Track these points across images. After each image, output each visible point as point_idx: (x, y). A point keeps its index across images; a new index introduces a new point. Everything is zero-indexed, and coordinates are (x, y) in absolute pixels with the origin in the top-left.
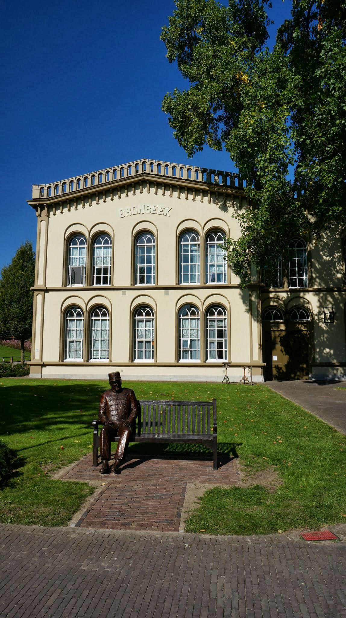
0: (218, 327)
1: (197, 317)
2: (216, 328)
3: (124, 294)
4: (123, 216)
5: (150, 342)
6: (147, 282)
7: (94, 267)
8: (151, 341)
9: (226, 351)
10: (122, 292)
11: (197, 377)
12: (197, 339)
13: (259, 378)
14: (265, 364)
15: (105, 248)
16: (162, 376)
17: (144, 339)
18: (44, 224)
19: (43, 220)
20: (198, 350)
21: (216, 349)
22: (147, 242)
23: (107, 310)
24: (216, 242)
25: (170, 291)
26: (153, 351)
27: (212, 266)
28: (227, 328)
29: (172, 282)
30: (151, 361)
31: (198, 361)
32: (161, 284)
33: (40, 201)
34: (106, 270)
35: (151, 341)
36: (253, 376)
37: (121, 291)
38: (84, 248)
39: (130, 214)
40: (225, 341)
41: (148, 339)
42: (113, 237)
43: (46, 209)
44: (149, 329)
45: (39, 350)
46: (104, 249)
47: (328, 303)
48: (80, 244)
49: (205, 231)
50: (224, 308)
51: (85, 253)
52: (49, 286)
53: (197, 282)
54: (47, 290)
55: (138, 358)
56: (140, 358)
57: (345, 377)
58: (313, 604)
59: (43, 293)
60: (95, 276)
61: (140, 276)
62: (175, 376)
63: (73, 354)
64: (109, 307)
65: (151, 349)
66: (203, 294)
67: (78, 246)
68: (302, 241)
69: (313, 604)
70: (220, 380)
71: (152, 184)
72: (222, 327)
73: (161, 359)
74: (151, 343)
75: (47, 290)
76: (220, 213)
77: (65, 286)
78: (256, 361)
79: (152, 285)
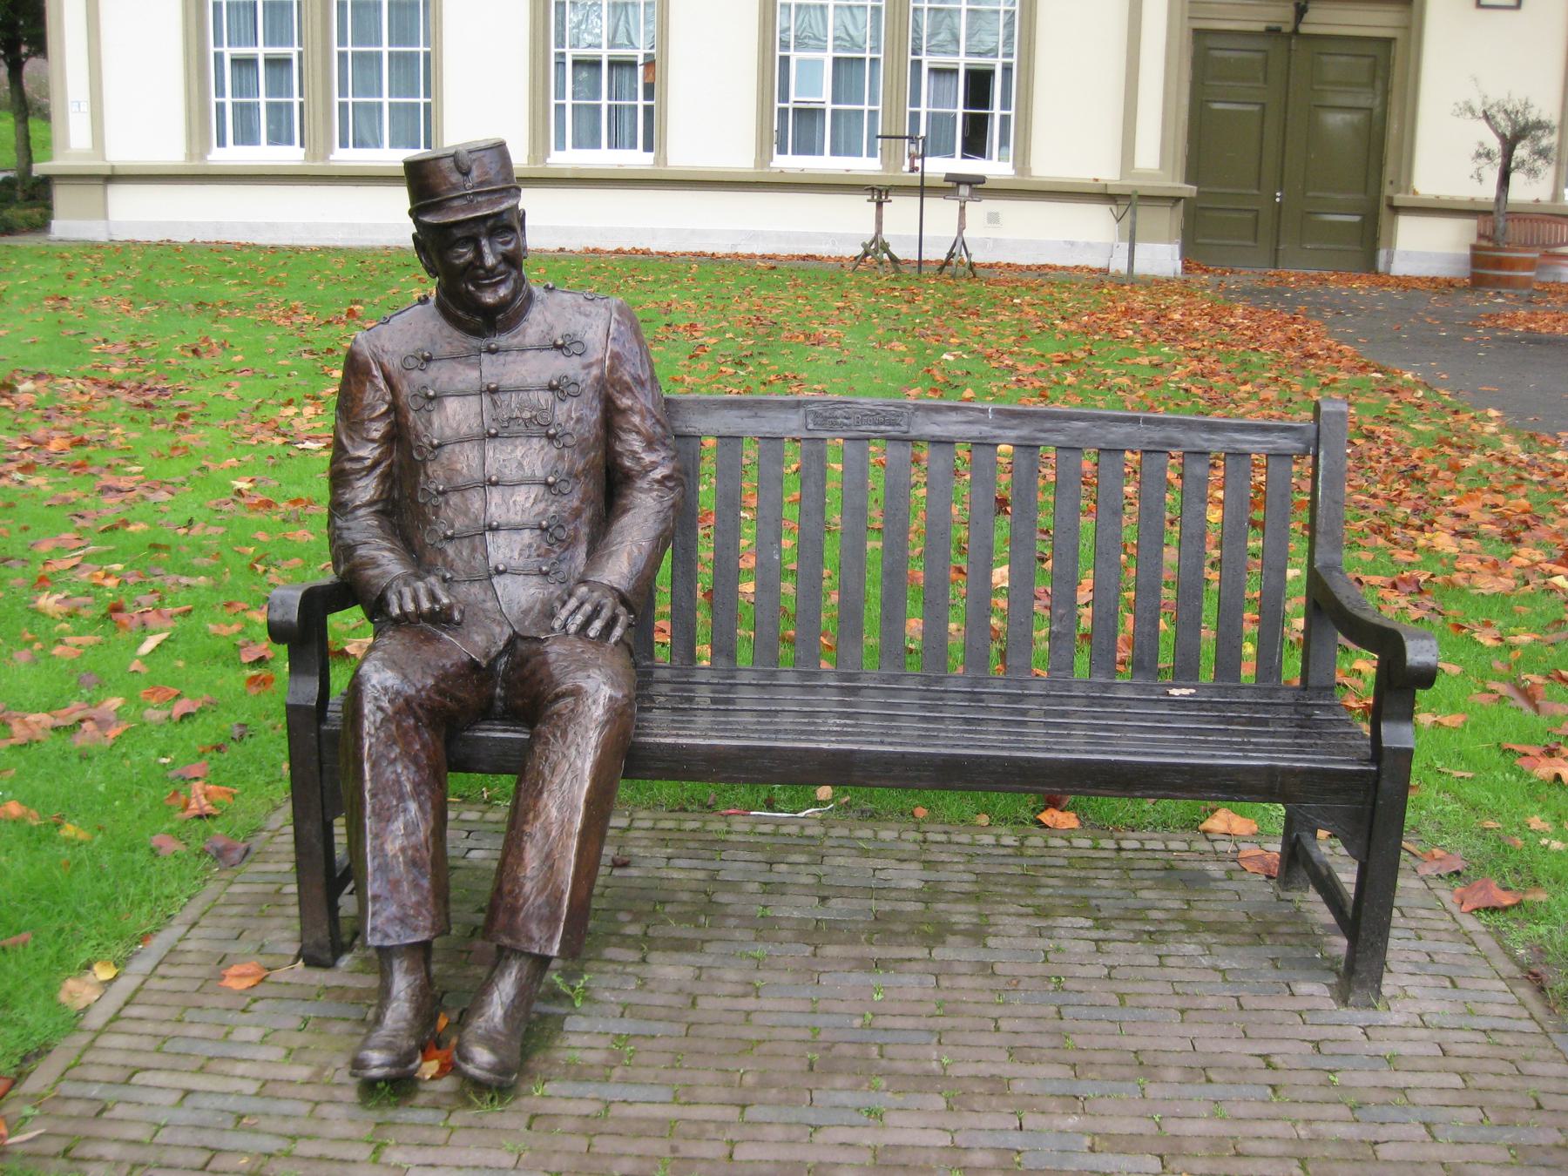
5: (633, 65)
8: (640, 61)
12: (868, 55)
14: (1190, 190)
16: (693, 232)
17: (605, 54)
20: (873, 60)
21: (960, 110)
26: (649, 111)
30: (636, 159)
35: (640, 61)
36: (1139, 247)
41: (622, 52)
47: (1544, 558)
57: (1566, 436)
58: (1519, 999)
60: (296, 100)
65: (641, 103)
69: (1519, 999)
74: (641, 70)
78: (1148, 175)
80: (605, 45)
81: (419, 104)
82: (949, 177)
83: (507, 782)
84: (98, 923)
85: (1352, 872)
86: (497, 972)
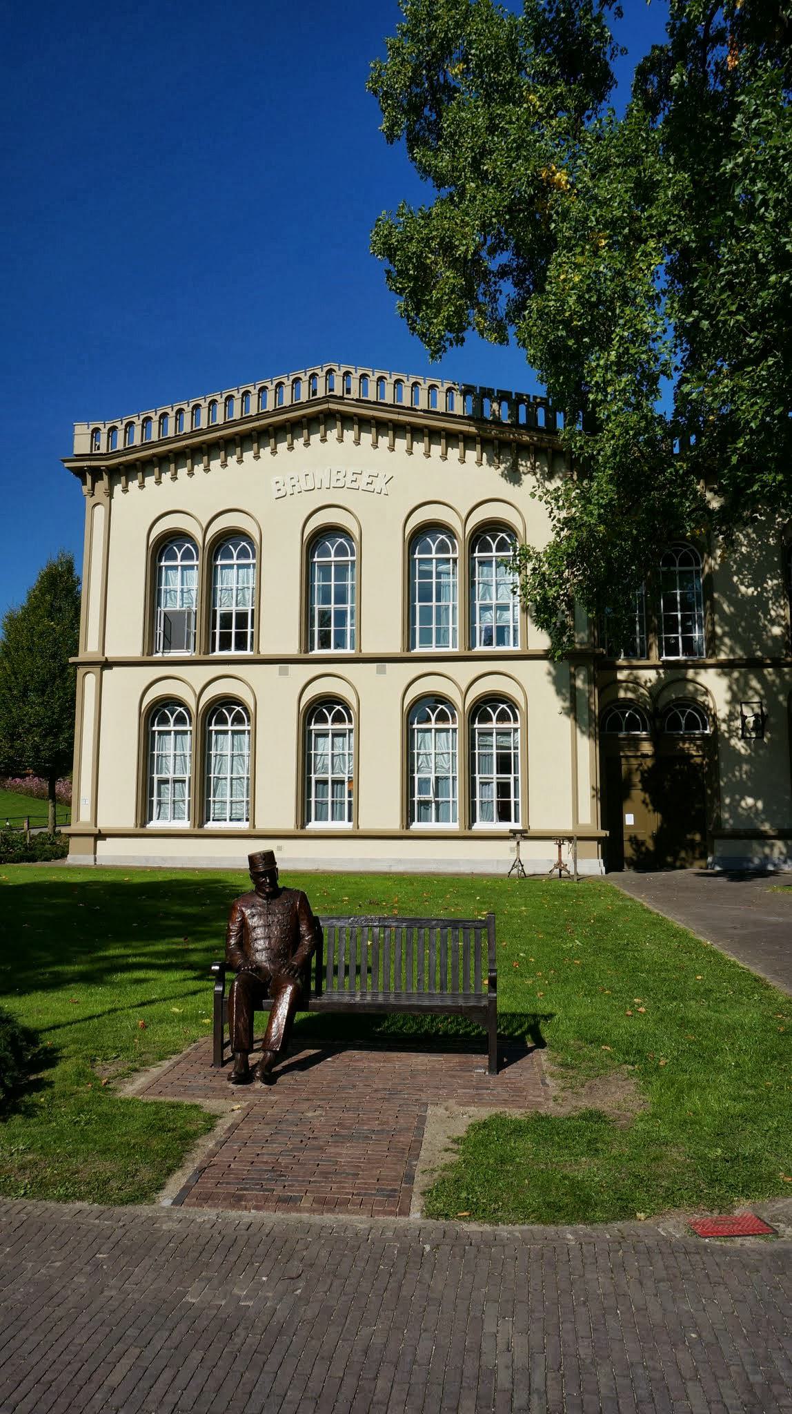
0: (498, 747)
1: (450, 726)
2: (494, 751)
3: (283, 673)
4: (282, 493)
5: (342, 782)
6: (337, 646)
7: (215, 612)
8: (346, 780)
9: (516, 804)
10: (280, 668)
11: (450, 862)
12: (451, 775)
13: (592, 865)
14: (605, 833)
15: (240, 566)
16: (372, 860)
17: (329, 776)
18: (100, 512)
19: (98, 504)
21: (495, 799)
22: (337, 554)
23: (246, 709)
24: (494, 553)
25: (388, 665)
26: (350, 803)
27: (486, 608)
28: (519, 751)
29: (395, 646)
30: (345, 826)
31: (453, 826)
32: (368, 649)
33: (90, 460)
34: (242, 618)
35: (346, 780)
36: (578, 861)
37: (278, 666)
38: (191, 567)
39: (296, 489)
40: (516, 780)
41: (338, 776)
42: (258, 541)
43: (105, 477)
44: (341, 752)
45: (89, 802)
46: (238, 569)
48: (183, 559)
49: (468, 528)
50: (513, 705)
51: (194, 580)
52: (111, 653)
53: (451, 645)
54: (107, 665)
55: (316, 820)
56: (320, 820)
59: (97, 670)
61: (320, 631)
62: (400, 861)
63: (168, 809)
64: (250, 702)
65: (346, 799)
66: (464, 672)
67: (178, 562)
68: (692, 551)
70: (504, 869)
71: (347, 420)
72: (509, 748)
73: (367, 822)
74: (346, 784)
75: (107, 665)
76: (504, 488)
77: (148, 655)
78: (585, 826)
79: (348, 651)
80: (317, 776)
81: (432, 607)
82: (511, 831)
83: (268, 1013)
84: (470, 43)
85: (282, 859)
86: (246, 948)
